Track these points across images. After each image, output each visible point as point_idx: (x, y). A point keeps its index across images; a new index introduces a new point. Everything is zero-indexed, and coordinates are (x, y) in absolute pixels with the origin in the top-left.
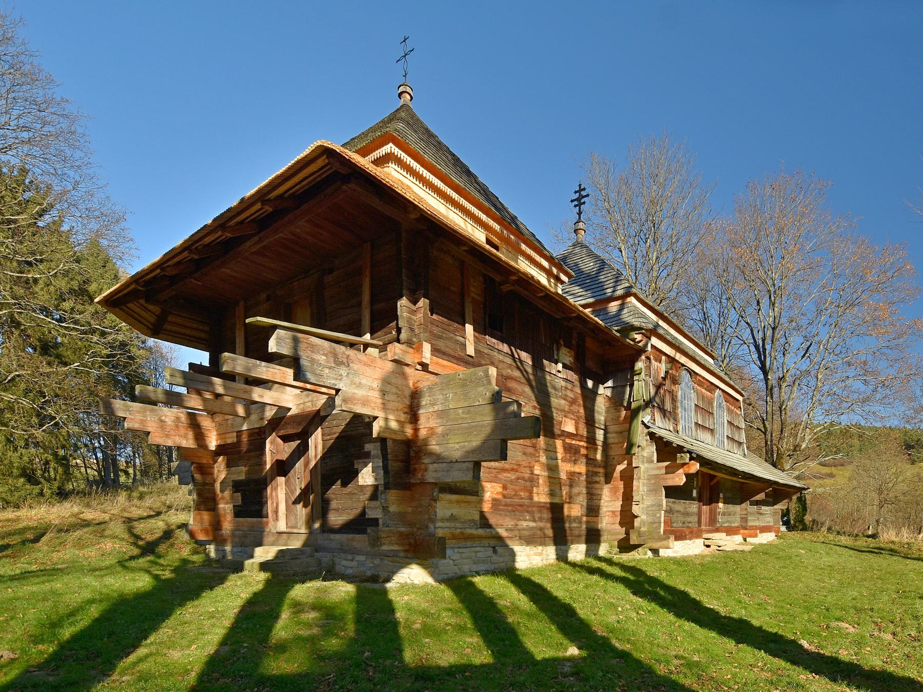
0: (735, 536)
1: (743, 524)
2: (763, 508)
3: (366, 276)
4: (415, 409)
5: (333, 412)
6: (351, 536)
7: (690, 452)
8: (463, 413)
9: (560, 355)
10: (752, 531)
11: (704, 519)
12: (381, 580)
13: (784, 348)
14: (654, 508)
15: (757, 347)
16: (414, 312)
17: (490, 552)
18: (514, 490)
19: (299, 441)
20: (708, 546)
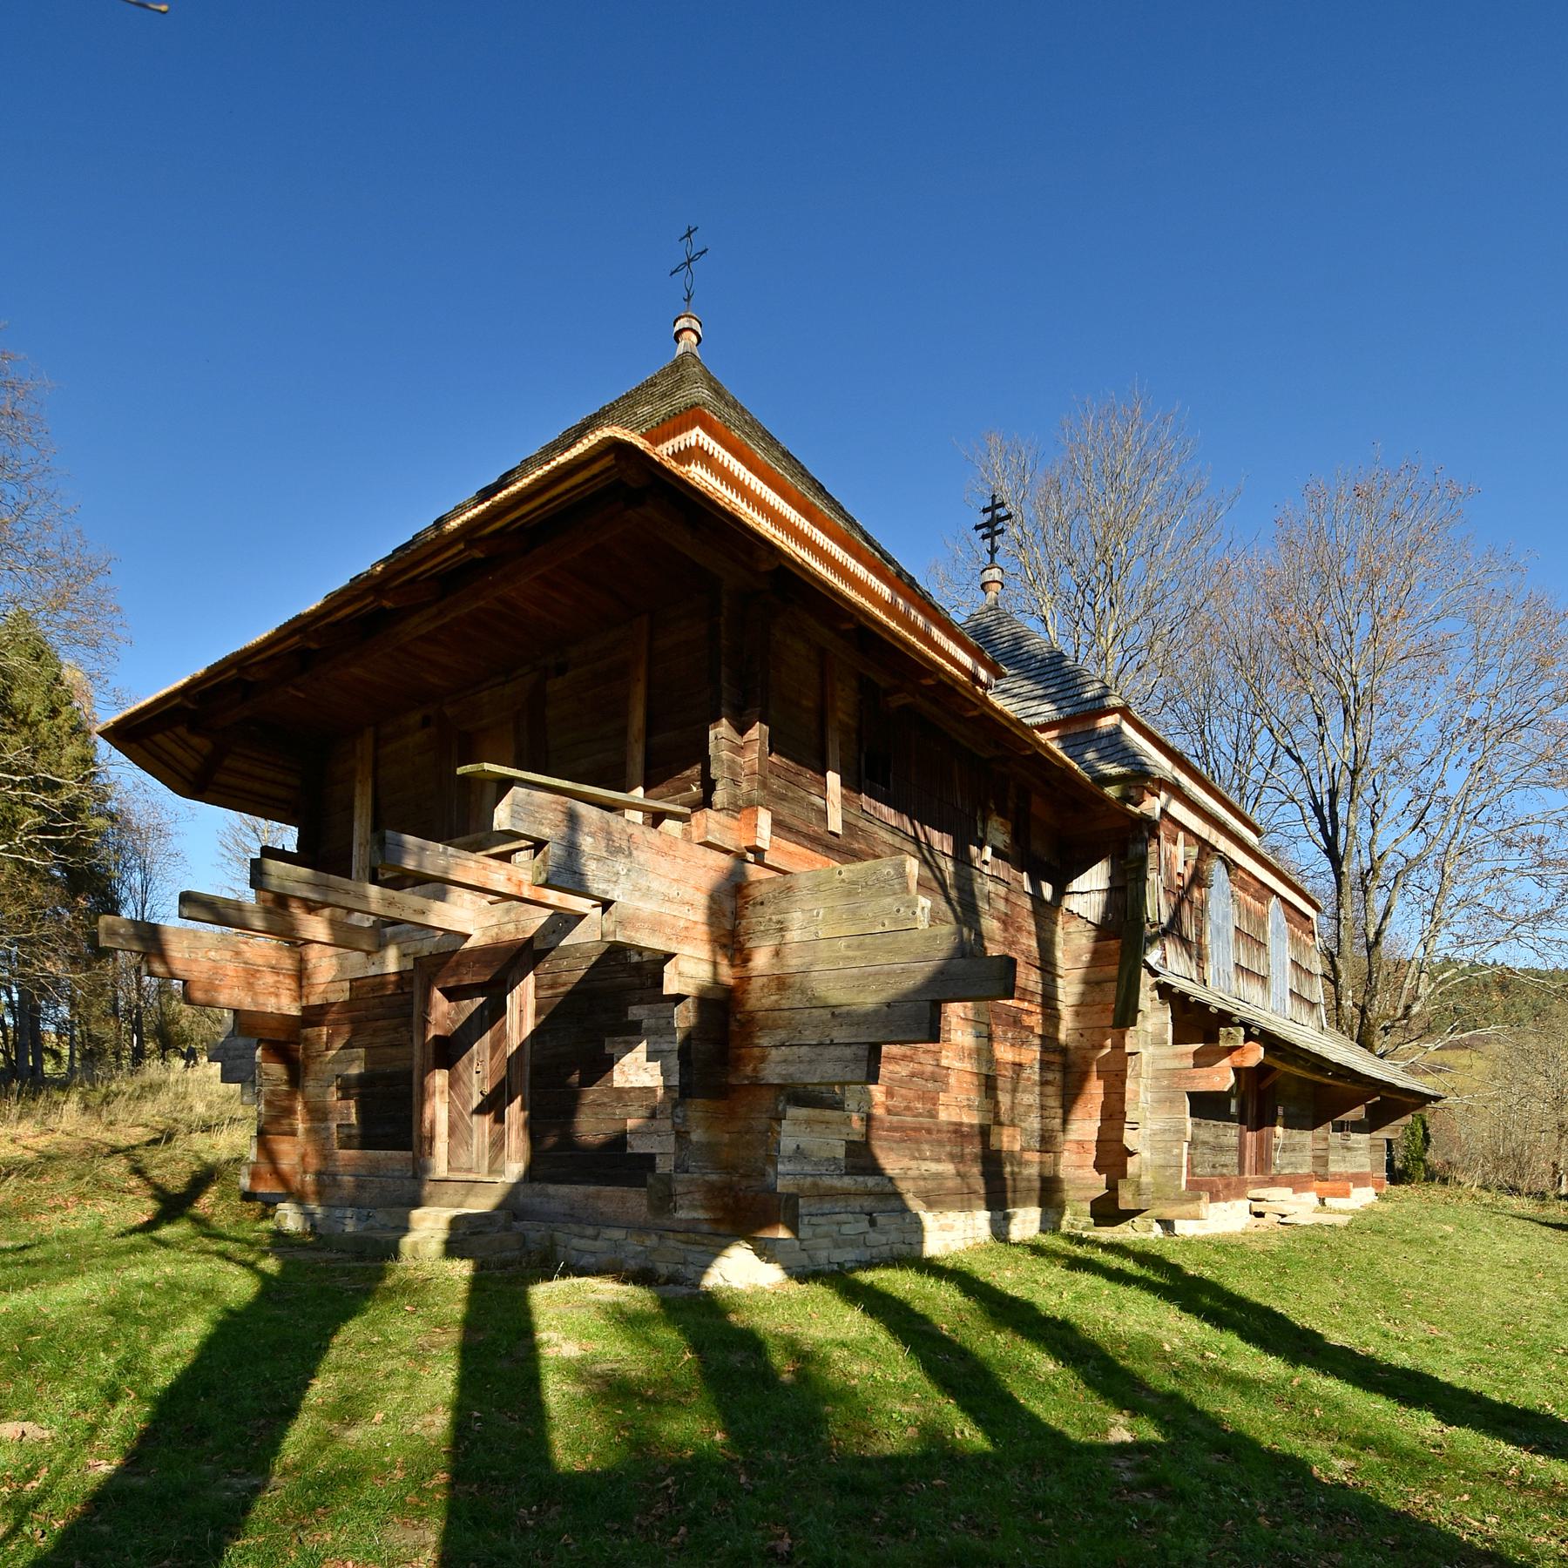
0: (1304, 1194)
1: (1317, 1169)
2: (1354, 1136)
3: (639, 680)
4: (741, 939)
5: (562, 944)
6: (592, 1189)
7: (1246, 1025)
8: (848, 947)
9: (989, 829)
10: (1338, 1185)
11: (1250, 1154)
12: (661, 1280)
13: (1372, 812)
14: (1167, 1137)
15: (1318, 809)
16: (739, 750)
17: (864, 1225)
18: (904, 1098)
19: (481, 1000)
20: (1260, 1215)
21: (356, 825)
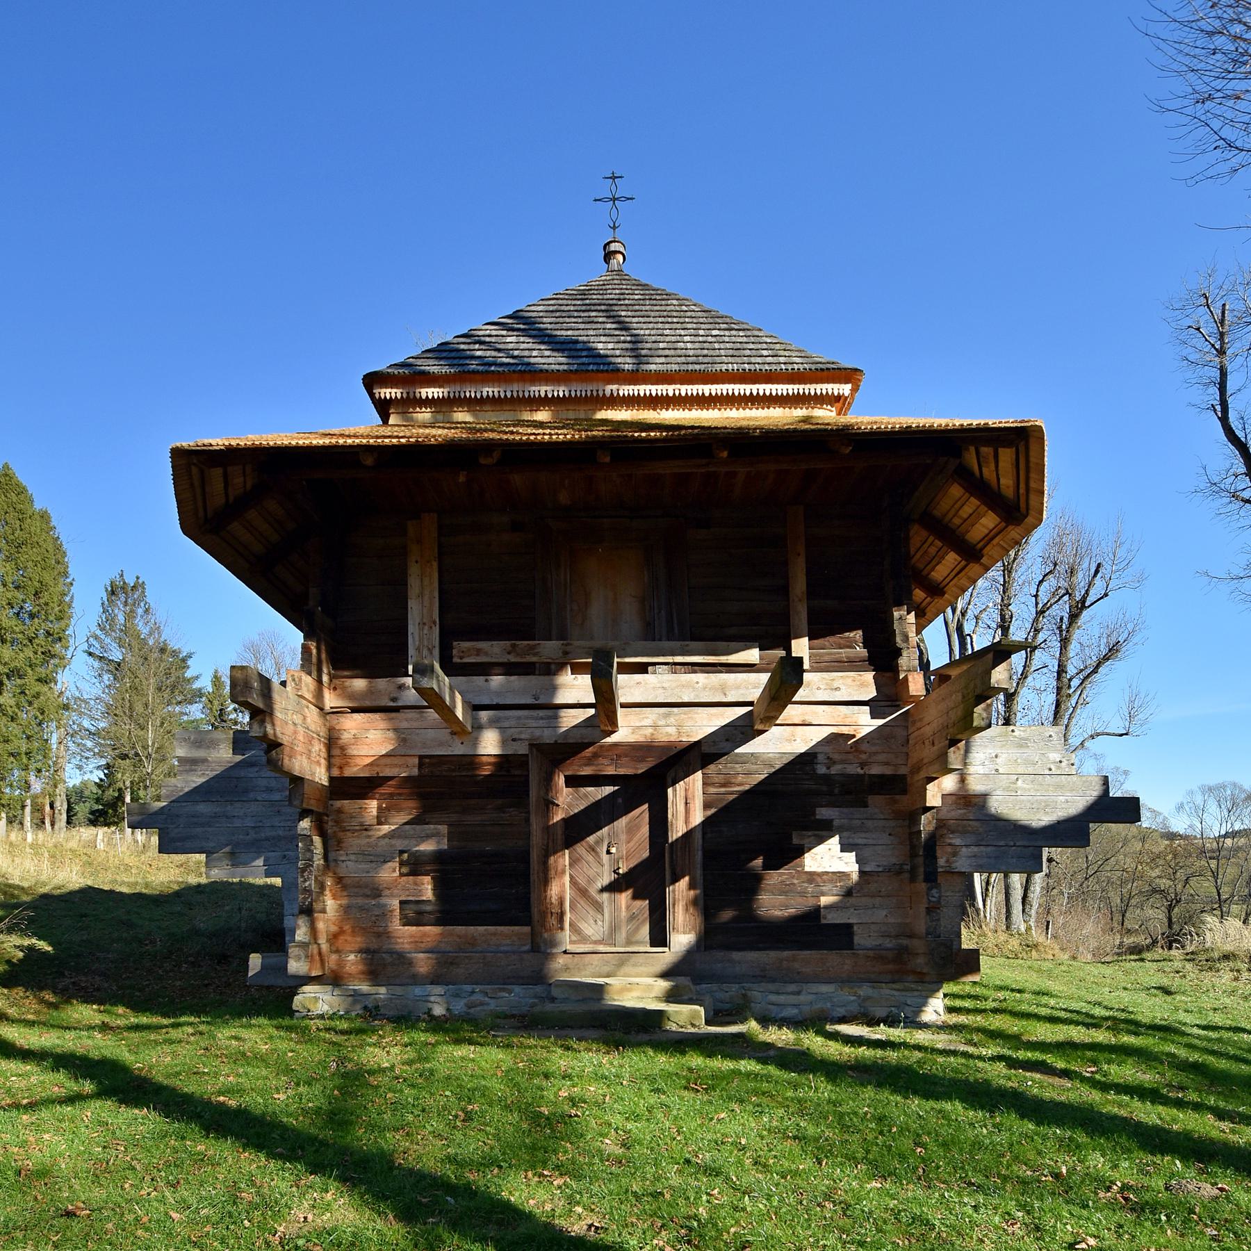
3: (799, 555)
6: (786, 954)
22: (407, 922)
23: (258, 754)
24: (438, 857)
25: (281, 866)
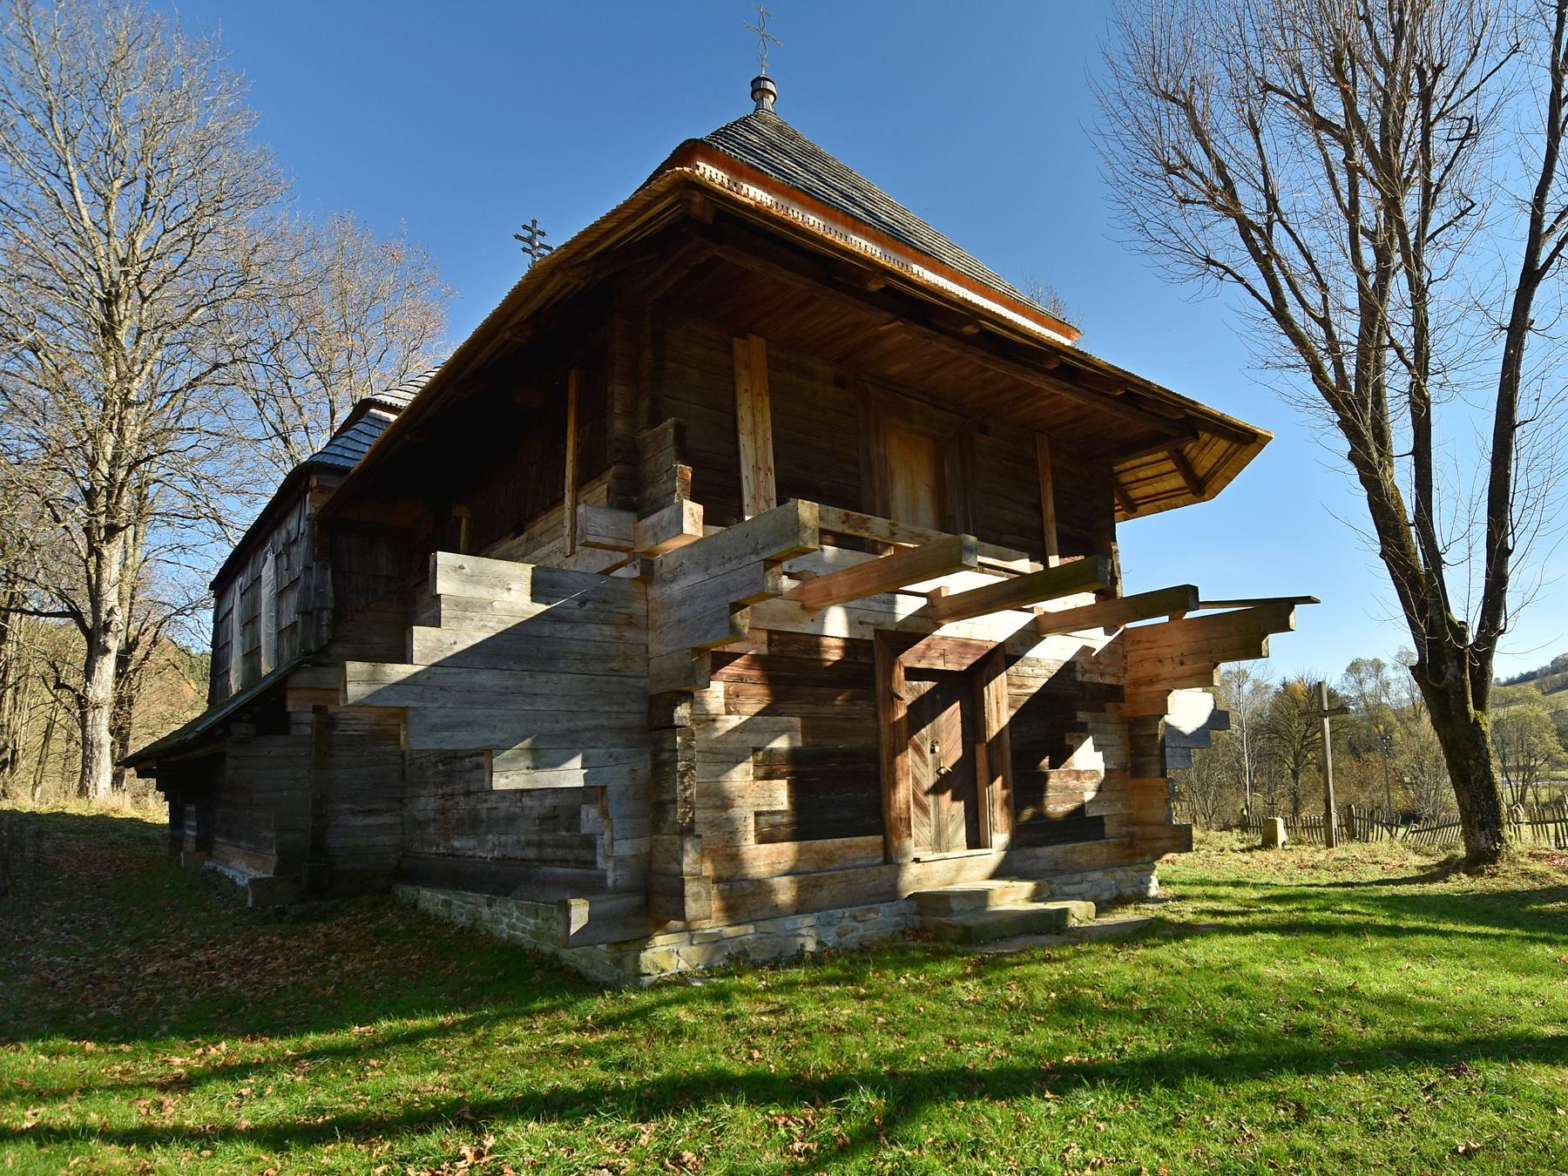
6: (1069, 846)
21: (745, 441)
22: (763, 838)
23: (569, 605)
24: (793, 755)
25: (606, 769)
